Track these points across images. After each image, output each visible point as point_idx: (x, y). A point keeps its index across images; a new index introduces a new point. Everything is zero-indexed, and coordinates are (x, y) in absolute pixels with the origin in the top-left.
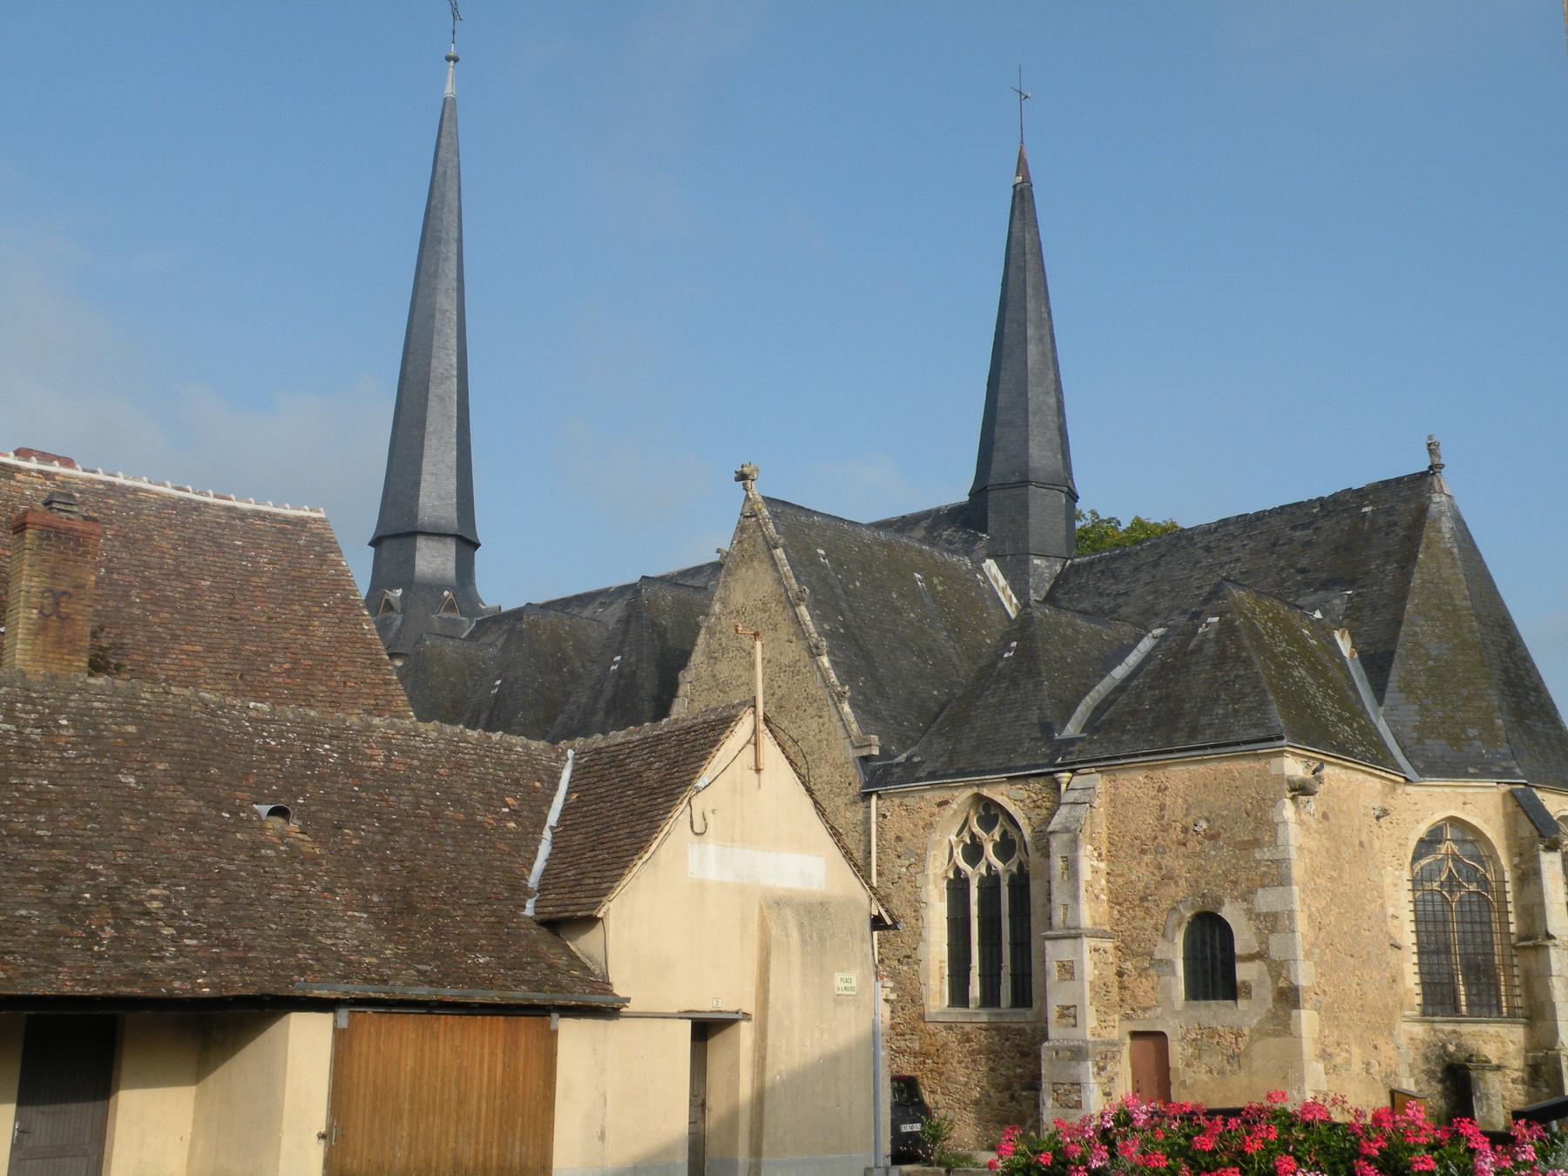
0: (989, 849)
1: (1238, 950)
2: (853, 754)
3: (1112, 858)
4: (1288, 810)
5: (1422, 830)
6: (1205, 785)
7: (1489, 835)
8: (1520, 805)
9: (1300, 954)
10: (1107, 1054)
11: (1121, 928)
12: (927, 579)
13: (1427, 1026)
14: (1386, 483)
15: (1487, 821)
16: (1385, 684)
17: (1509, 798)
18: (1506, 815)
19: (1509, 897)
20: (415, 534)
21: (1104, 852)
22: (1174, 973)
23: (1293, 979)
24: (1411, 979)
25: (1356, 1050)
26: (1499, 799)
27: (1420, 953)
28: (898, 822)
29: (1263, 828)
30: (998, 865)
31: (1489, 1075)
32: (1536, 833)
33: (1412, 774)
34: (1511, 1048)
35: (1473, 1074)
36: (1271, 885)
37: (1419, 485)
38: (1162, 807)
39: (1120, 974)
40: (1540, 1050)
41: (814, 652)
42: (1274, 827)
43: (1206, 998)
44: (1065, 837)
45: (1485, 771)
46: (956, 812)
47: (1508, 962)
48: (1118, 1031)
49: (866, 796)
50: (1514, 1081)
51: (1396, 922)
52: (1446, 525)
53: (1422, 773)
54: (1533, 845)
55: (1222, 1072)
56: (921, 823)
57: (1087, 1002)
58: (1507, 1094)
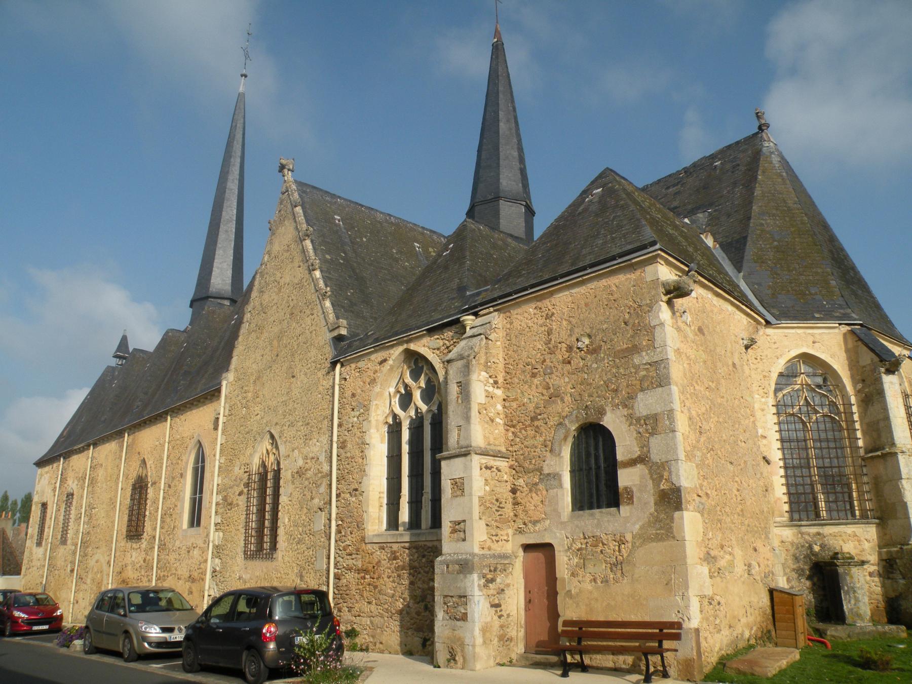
0: (417, 395)
1: (620, 457)
2: (330, 336)
3: (508, 385)
5: (780, 366)
6: (586, 305)
7: (835, 367)
8: (860, 340)
9: (682, 455)
10: (494, 569)
11: (515, 448)
13: (795, 530)
14: (729, 147)
16: (742, 258)
17: (849, 337)
18: (847, 351)
19: (856, 417)
20: (207, 298)
21: (500, 380)
22: (561, 486)
23: (674, 479)
24: (780, 491)
25: (738, 552)
26: (840, 338)
27: (786, 467)
28: (355, 384)
29: (642, 331)
30: (424, 408)
31: (854, 570)
32: (876, 359)
34: (867, 545)
35: (841, 570)
38: (549, 332)
39: (514, 491)
40: (894, 545)
41: (311, 270)
42: (650, 331)
44: (460, 364)
45: (828, 316)
46: (392, 367)
47: (859, 471)
48: (510, 544)
49: (334, 364)
50: (871, 574)
51: (764, 441)
52: (775, 159)
54: (874, 370)
55: (605, 581)
56: (368, 380)
57: (476, 515)
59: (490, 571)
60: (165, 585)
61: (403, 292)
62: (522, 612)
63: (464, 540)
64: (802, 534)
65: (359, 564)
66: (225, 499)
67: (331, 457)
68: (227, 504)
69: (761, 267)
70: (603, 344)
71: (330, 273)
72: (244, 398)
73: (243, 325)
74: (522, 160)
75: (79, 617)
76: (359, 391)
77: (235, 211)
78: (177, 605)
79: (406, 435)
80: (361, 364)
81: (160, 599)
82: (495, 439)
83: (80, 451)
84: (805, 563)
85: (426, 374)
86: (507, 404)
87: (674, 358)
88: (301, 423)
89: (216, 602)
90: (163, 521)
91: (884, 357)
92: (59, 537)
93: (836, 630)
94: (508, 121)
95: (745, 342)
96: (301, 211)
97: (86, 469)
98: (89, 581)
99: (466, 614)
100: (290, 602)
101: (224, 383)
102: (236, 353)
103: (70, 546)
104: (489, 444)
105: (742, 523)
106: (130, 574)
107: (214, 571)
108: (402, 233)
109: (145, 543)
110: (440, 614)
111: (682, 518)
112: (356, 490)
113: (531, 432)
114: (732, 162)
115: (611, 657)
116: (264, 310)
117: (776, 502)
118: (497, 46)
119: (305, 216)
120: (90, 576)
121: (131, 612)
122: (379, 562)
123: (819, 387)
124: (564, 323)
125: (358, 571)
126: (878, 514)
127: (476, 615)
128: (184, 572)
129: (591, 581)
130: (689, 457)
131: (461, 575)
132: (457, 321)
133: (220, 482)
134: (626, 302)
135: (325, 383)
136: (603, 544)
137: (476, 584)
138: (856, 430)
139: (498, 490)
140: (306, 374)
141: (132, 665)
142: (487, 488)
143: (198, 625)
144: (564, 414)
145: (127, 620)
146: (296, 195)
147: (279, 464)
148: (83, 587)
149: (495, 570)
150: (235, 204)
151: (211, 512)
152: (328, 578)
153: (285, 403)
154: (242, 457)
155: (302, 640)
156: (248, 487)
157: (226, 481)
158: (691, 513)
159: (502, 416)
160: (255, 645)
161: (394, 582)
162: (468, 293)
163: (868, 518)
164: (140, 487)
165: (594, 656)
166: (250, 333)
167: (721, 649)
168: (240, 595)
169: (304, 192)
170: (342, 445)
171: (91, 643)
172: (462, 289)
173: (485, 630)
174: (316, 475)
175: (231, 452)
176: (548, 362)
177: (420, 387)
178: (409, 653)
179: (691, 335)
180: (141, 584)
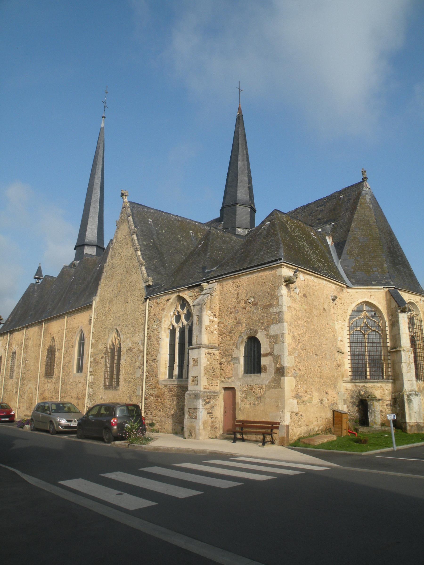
0: (183, 317)
1: (263, 352)
2: (144, 285)
3: (220, 317)
4: (284, 290)
5: (353, 306)
6: (253, 283)
7: (380, 308)
9: (286, 352)
10: (210, 397)
12: (195, 233)
13: (353, 384)
14: (348, 188)
15: (379, 303)
16: (342, 252)
18: (387, 300)
19: (388, 332)
20: (84, 245)
21: (217, 314)
22: (239, 363)
23: (282, 363)
26: (384, 294)
29: (274, 298)
30: (185, 323)
31: (375, 403)
32: (397, 306)
33: (349, 284)
34: (386, 392)
35: (369, 403)
36: (276, 323)
37: (359, 186)
38: (238, 294)
39: (221, 364)
41: (136, 251)
43: (251, 373)
44: (198, 307)
45: (379, 283)
46: (172, 303)
48: (218, 387)
49: (146, 299)
50: (387, 405)
51: (342, 343)
52: (368, 198)
53: (353, 284)
54: (396, 311)
55: (254, 404)
56: (161, 308)
57: (202, 374)
58: (384, 410)
59: (208, 398)
60: (66, 400)
61: (183, 259)
62: (222, 417)
63: (197, 385)
64: (356, 386)
65: (156, 393)
66: (95, 360)
67: (144, 343)
68: (95, 362)
69: (350, 257)
70: (259, 302)
71: (145, 252)
72: (104, 311)
73: (103, 274)
74: (250, 182)
75: (21, 415)
76: (157, 313)
77: (99, 196)
78: (72, 410)
79: (177, 335)
80: (158, 300)
81: (65, 407)
82: (213, 341)
83: (19, 330)
84: (356, 399)
85: (187, 307)
86: (219, 325)
87: (287, 310)
88: (130, 326)
89: (90, 409)
90: (63, 369)
91: (400, 305)
92: (9, 374)
93: (363, 429)
94: (243, 160)
95: (332, 298)
96: (132, 219)
97: (22, 340)
98: (25, 398)
99: (196, 416)
100: (123, 410)
101: (94, 302)
102: (100, 287)
103: (14, 379)
104: (210, 343)
105: (320, 381)
106: (47, 394)
107: (90, 395)
108: (183, 225)
109: (54, 380)
110: (186, 416)
111: (284, 379)
112: (155, 359)
113: (228, 338)
114: (348, 197)
115: (255, 436)
116: (113, 267)
117: (345, 371)
118: (239, 117)
119: (134, 221)
120: (26, 395)
121: (53, 412)
122: (164, 393)
123: (372, 316)
124: (244, 290)
125: (155, 396)
126: (393, 378)
127: (201, 417)
128: (74, 394)
129: (249, 404)
130: (291, 353)
131: (195, 400)
132: (199, 285)
133: (92, 351)
134: (269, 284)
135: (142, 307)
136: (255, 389)
137: (201, 404)
138: (387, 338)
139: (213, 363)
140: (133, 302)
141: (54, 435)
142: (208, 363)
143: (84, 419)
144: (242, 331)
145: (51, 416)
146: (129, 210)
147: (120, 344)
148: (23, 400)
149: (210, 398)
150: (99, 192)
151: (88, 366)
152: (142, 399)
153: (123, 315)
154: (103, 340)
155: (128, 425)
156: (106, 354)
157: (95, 351)
158: (289, 378)
159: (217, 330)
160: (108, 427)
161: (170, 402)
162: (206, 271)
163: (388, 379)
164: (51, 352)
165: (248, 436)
166: (107, 278)
167: (300, 434)
168: (102, 407)
169: (133, 207)
170: (149, 338)
171: (34, 426)
172: (204, 268)
173: (204, 423)
174: (137, 351)
175: (97, 337)
176: (237, 308)
177: (184, 313)
178: (176, 433)
179: (298, 299)
180: (53, 400)
